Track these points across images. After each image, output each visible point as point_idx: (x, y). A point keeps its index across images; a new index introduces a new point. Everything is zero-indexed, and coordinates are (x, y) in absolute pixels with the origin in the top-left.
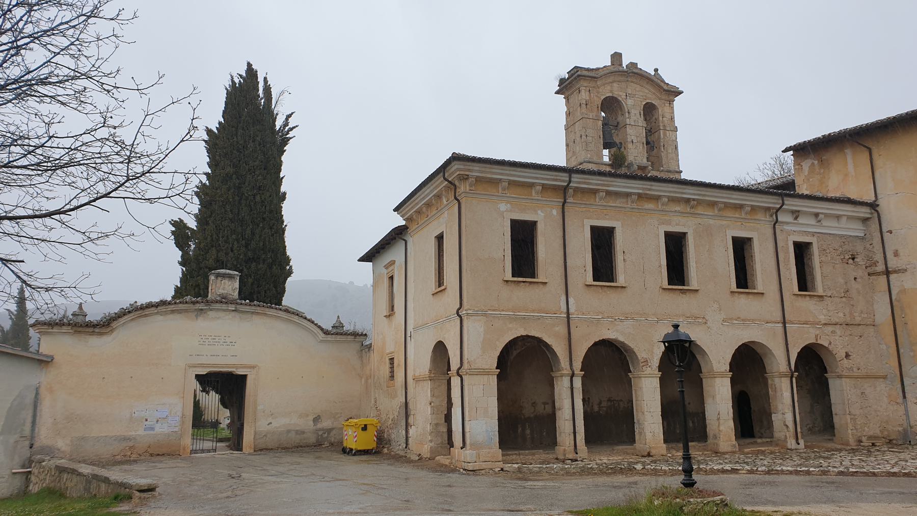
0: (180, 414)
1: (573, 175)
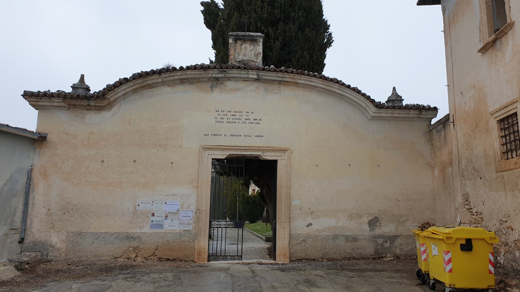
0: (193, 208)
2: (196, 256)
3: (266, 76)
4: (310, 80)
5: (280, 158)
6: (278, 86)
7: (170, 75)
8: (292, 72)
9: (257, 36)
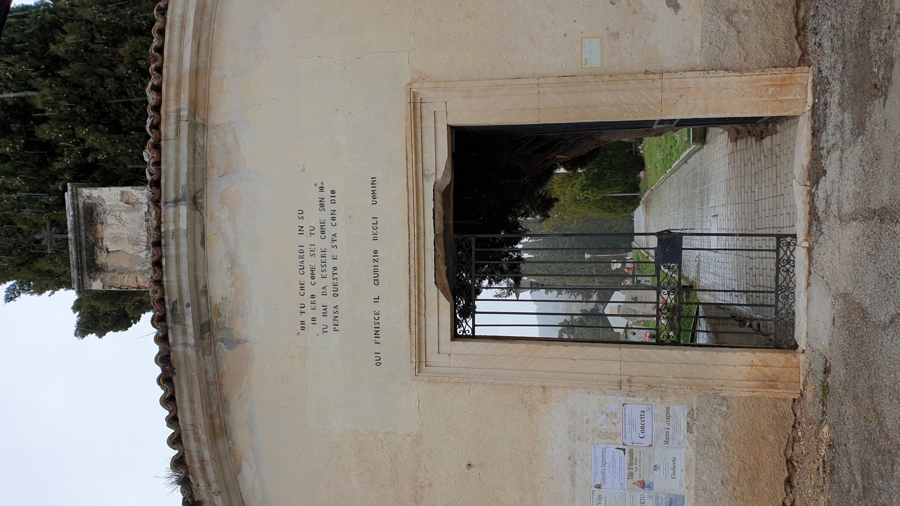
0: (613, 402)
1: (773, 295)
2: (780, 393)
3: (177, 174)
4: (177, 25)
5: (441, 116)
6: (211, 132)
7: (199, 473)
8: (158, 89)
9: (75, 207)
